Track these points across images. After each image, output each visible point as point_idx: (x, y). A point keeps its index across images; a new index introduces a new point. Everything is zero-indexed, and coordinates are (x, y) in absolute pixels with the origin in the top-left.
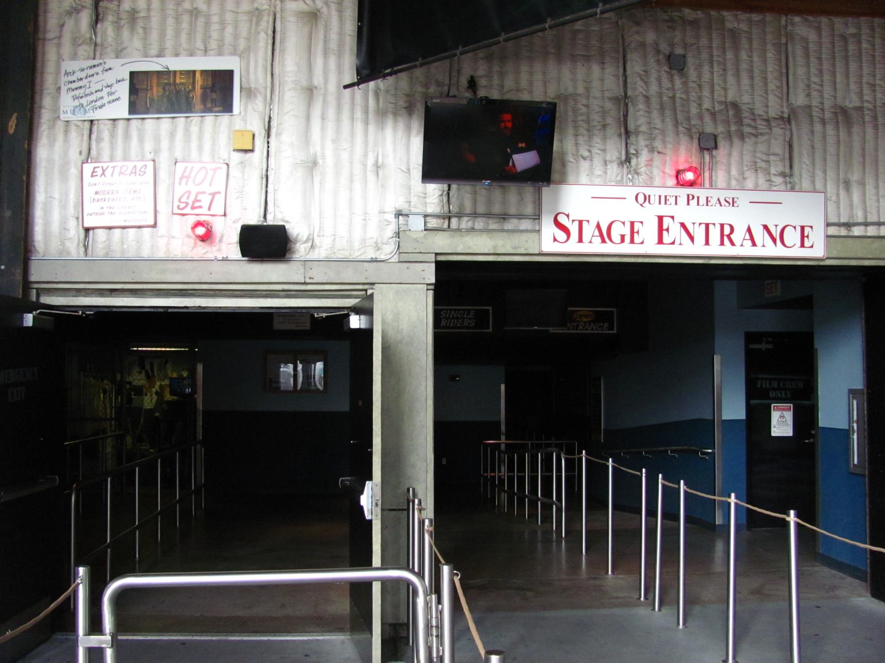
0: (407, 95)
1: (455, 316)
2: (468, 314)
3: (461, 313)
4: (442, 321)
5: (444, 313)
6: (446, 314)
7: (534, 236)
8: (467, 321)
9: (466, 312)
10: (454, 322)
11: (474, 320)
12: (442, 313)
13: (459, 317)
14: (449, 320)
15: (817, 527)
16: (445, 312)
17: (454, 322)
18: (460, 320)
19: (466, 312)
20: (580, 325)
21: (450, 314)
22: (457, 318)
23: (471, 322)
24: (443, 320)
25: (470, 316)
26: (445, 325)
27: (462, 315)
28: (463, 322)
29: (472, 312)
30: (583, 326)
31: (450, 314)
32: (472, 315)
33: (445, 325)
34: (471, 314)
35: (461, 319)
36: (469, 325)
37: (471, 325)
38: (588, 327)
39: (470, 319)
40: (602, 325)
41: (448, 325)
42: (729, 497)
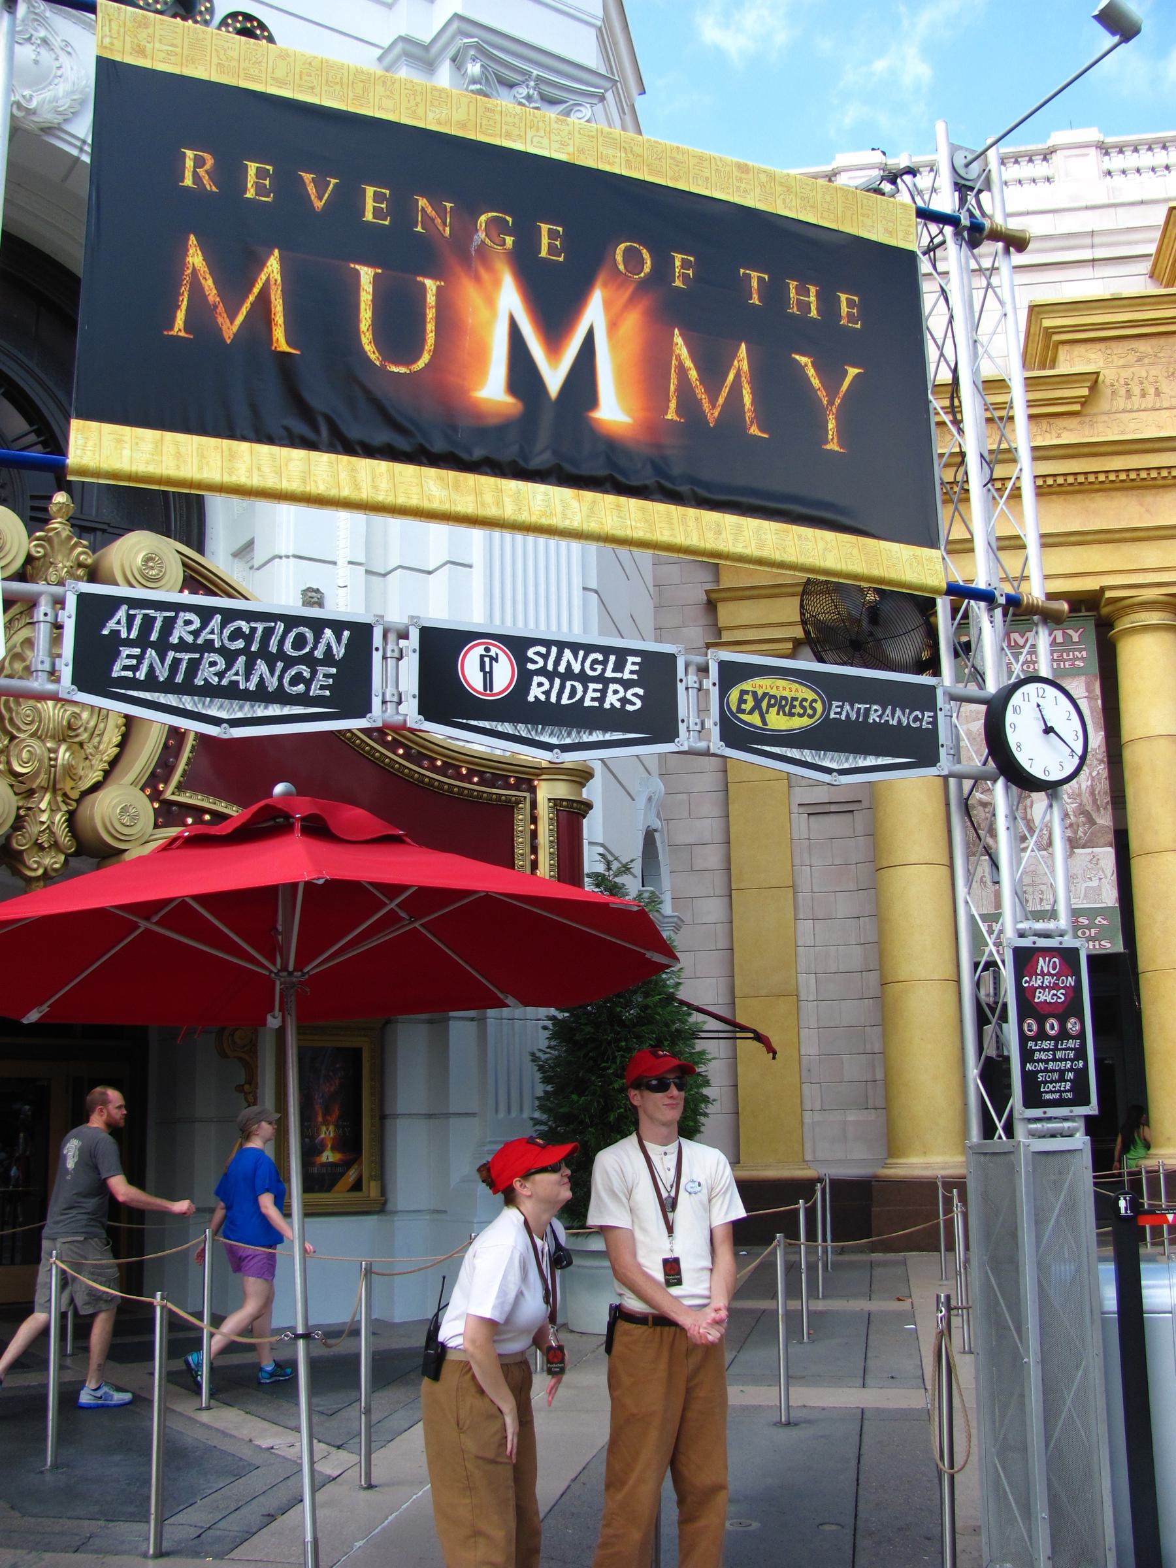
0: (539, 1070)
1: (576, 668)
2: (620, 667)
3: (595, 662)
4: (534, 684)
5: (537, 653)
6: (545, 657)
7: (246, 1105)
8: (616, 692)
9: (612, 658)
10: (573, 689)
11: (641, 692)
12: (530, 653)
13: (590, 673)
14: (557, 681)
15: (302, 1487)
16: (543, 650)
17: (573, 689)
18: (592, 686)
19: (612, 658)
20: (180, 622)
21: (557, 662)
22: (583, 678)
23: (629, 695)
24: (537, 679)
25: (627, 675)
26: (618, 705)
27: (599, 668)
28: (604, 692)
29: (631, 659)
30: (880, 713)
31: (557, 662)
32: (632, 672)
33: (542, 698)
34: (629, 667)
35: (595, 680)
36: (623, 706)
37: (629, 708)
38: (890, 719)
39: (627, 684)
40: (307, 674)
41: (553, 699)
42: (154, 1297)
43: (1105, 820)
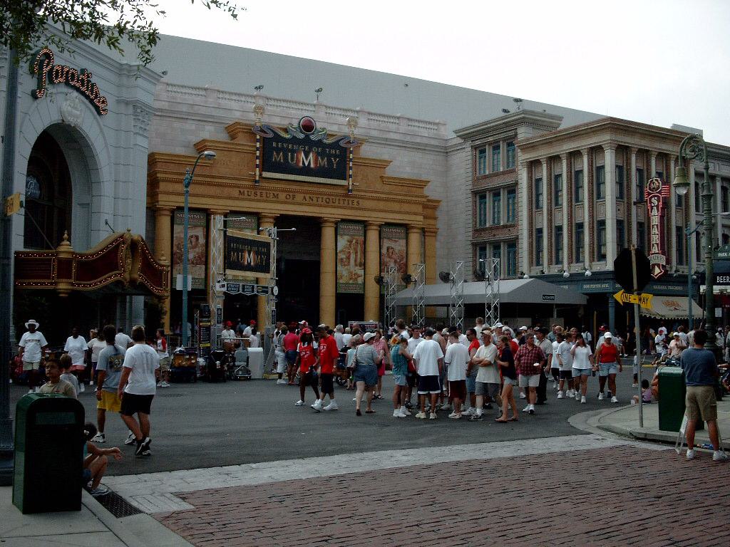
43: (203, 259)
